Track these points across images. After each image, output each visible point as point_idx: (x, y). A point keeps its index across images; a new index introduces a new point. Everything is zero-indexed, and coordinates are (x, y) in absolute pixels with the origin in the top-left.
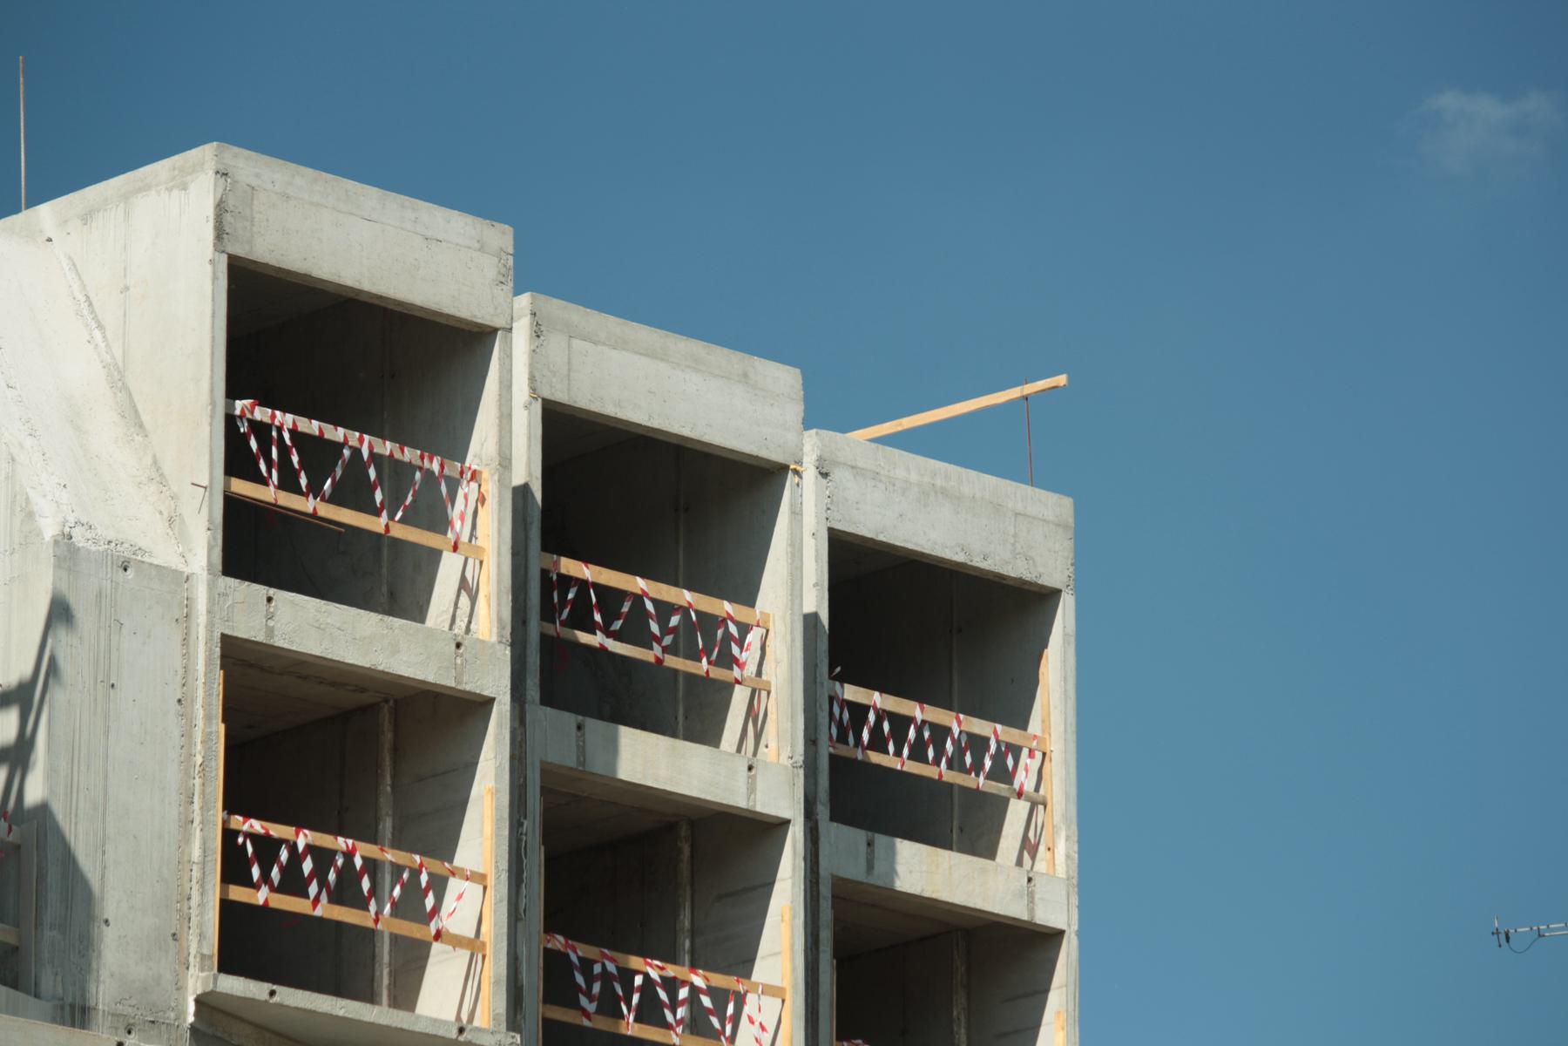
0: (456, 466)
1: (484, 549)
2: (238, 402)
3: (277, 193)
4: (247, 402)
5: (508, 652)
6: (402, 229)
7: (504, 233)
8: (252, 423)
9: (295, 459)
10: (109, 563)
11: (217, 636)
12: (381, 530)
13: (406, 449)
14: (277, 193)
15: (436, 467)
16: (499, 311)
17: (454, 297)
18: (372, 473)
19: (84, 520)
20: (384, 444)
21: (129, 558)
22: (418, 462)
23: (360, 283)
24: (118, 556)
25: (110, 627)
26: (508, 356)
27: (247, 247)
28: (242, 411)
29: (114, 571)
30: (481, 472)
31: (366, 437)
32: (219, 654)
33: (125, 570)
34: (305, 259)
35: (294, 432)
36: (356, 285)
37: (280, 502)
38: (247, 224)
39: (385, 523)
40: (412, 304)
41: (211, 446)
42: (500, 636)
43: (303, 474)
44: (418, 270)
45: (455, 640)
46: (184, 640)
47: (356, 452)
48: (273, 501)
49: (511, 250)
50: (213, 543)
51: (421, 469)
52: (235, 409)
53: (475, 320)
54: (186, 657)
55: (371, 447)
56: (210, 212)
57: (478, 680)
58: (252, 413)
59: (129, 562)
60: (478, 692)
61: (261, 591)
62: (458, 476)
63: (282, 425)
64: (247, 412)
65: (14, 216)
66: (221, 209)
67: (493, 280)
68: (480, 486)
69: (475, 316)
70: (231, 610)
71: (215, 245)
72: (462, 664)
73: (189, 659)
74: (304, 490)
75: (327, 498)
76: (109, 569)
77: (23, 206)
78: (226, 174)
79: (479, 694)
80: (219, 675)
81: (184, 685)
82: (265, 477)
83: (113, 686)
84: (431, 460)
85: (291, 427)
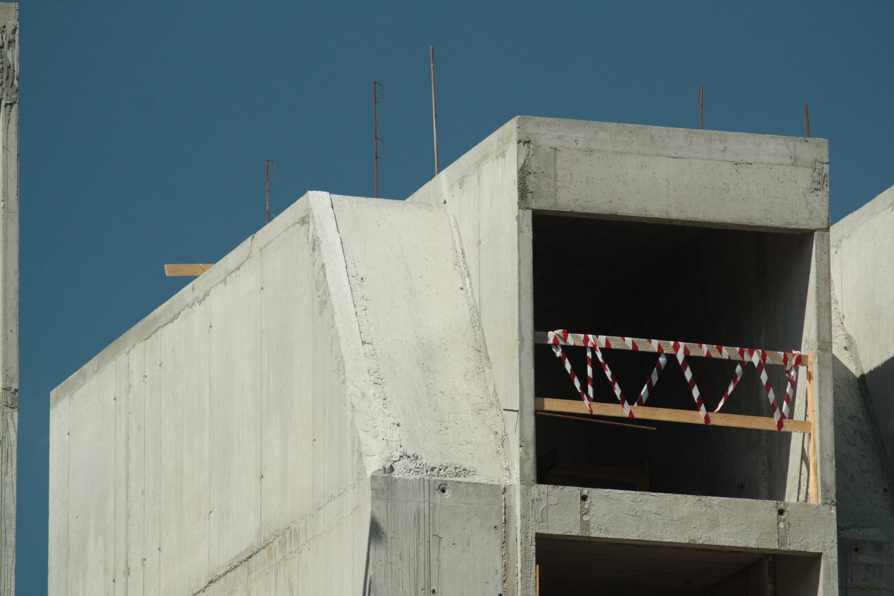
0: (779, 356)
1: (810, 423)
2: (550, 333)
3: (580, 150)
4: (559, 332)
5: (834, 511)
6: (711, 159)
7: (818, 146)
8: (567, 349)
9: (608, 373)
10: (426, 488)
11: (532, 536)
12: (701, 421)
13: (724, 349)
14: (580, 150)
15: (756, 359)
16: (814, 215)
17: (766, 210)
18: (688, 374)
19: (410, 453)
20: (701, 347)
21: (446, 481)
22: (739, 358)
23: (668, 213)
24: (435, 481)
25: (429, 542)
26: (825, 253)
27: (551, 201)
28: (555, 339)
29: (432, 494)
30: (807, 357)
31: (682, 344)
32: (534, 552)
33: (444, 491)
34: (611, 202)
35: (606, 351)
36: (664, 216)
37: (595, 412)
38: (551, 181)
39: (704, 415)
40: (722, 223)
41: (520, 375)
42: (825, 498)
43: (616, 386)
44: (728, 192)
45: (777, 507)
46: (503, 543)
47: (672, 358)
48: (589, 413)
49: (826, 160)
50: (525, 457)
51: (742, 363)
52: (547, 339)
53: (789, 227)
54: (506, 557)
55: (686, 351)
56: (514, 176)
57: (804, 539)
58: (565, 340)
59: (446, 485)
60: (803, 550)
61: (574, 492)
62: (782, 363)
63: (595, 346)
64: (560, 340)
65: (430, 182)
66: (523, 173)
67: (808, 189)
68: (807, 367)
69: (789, 223)
70: (545, 511)
71: (519, 203)
72: (785, 528)
73: (508, 558)
74: (619, 398)
75: (644, 401)
76: (426, 494)
77: (436, 173)
78: (529, 142)
79: (805, 552)
80: (534, 570)
81: (505, 581)
82: (579, 392)
83: (434, 591)
84: (751, 354)
85: (604, 346)
